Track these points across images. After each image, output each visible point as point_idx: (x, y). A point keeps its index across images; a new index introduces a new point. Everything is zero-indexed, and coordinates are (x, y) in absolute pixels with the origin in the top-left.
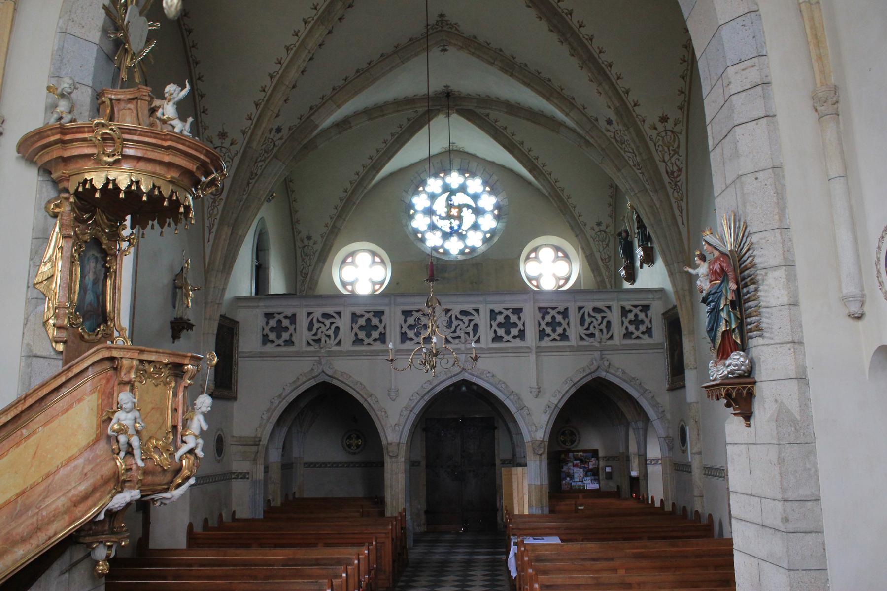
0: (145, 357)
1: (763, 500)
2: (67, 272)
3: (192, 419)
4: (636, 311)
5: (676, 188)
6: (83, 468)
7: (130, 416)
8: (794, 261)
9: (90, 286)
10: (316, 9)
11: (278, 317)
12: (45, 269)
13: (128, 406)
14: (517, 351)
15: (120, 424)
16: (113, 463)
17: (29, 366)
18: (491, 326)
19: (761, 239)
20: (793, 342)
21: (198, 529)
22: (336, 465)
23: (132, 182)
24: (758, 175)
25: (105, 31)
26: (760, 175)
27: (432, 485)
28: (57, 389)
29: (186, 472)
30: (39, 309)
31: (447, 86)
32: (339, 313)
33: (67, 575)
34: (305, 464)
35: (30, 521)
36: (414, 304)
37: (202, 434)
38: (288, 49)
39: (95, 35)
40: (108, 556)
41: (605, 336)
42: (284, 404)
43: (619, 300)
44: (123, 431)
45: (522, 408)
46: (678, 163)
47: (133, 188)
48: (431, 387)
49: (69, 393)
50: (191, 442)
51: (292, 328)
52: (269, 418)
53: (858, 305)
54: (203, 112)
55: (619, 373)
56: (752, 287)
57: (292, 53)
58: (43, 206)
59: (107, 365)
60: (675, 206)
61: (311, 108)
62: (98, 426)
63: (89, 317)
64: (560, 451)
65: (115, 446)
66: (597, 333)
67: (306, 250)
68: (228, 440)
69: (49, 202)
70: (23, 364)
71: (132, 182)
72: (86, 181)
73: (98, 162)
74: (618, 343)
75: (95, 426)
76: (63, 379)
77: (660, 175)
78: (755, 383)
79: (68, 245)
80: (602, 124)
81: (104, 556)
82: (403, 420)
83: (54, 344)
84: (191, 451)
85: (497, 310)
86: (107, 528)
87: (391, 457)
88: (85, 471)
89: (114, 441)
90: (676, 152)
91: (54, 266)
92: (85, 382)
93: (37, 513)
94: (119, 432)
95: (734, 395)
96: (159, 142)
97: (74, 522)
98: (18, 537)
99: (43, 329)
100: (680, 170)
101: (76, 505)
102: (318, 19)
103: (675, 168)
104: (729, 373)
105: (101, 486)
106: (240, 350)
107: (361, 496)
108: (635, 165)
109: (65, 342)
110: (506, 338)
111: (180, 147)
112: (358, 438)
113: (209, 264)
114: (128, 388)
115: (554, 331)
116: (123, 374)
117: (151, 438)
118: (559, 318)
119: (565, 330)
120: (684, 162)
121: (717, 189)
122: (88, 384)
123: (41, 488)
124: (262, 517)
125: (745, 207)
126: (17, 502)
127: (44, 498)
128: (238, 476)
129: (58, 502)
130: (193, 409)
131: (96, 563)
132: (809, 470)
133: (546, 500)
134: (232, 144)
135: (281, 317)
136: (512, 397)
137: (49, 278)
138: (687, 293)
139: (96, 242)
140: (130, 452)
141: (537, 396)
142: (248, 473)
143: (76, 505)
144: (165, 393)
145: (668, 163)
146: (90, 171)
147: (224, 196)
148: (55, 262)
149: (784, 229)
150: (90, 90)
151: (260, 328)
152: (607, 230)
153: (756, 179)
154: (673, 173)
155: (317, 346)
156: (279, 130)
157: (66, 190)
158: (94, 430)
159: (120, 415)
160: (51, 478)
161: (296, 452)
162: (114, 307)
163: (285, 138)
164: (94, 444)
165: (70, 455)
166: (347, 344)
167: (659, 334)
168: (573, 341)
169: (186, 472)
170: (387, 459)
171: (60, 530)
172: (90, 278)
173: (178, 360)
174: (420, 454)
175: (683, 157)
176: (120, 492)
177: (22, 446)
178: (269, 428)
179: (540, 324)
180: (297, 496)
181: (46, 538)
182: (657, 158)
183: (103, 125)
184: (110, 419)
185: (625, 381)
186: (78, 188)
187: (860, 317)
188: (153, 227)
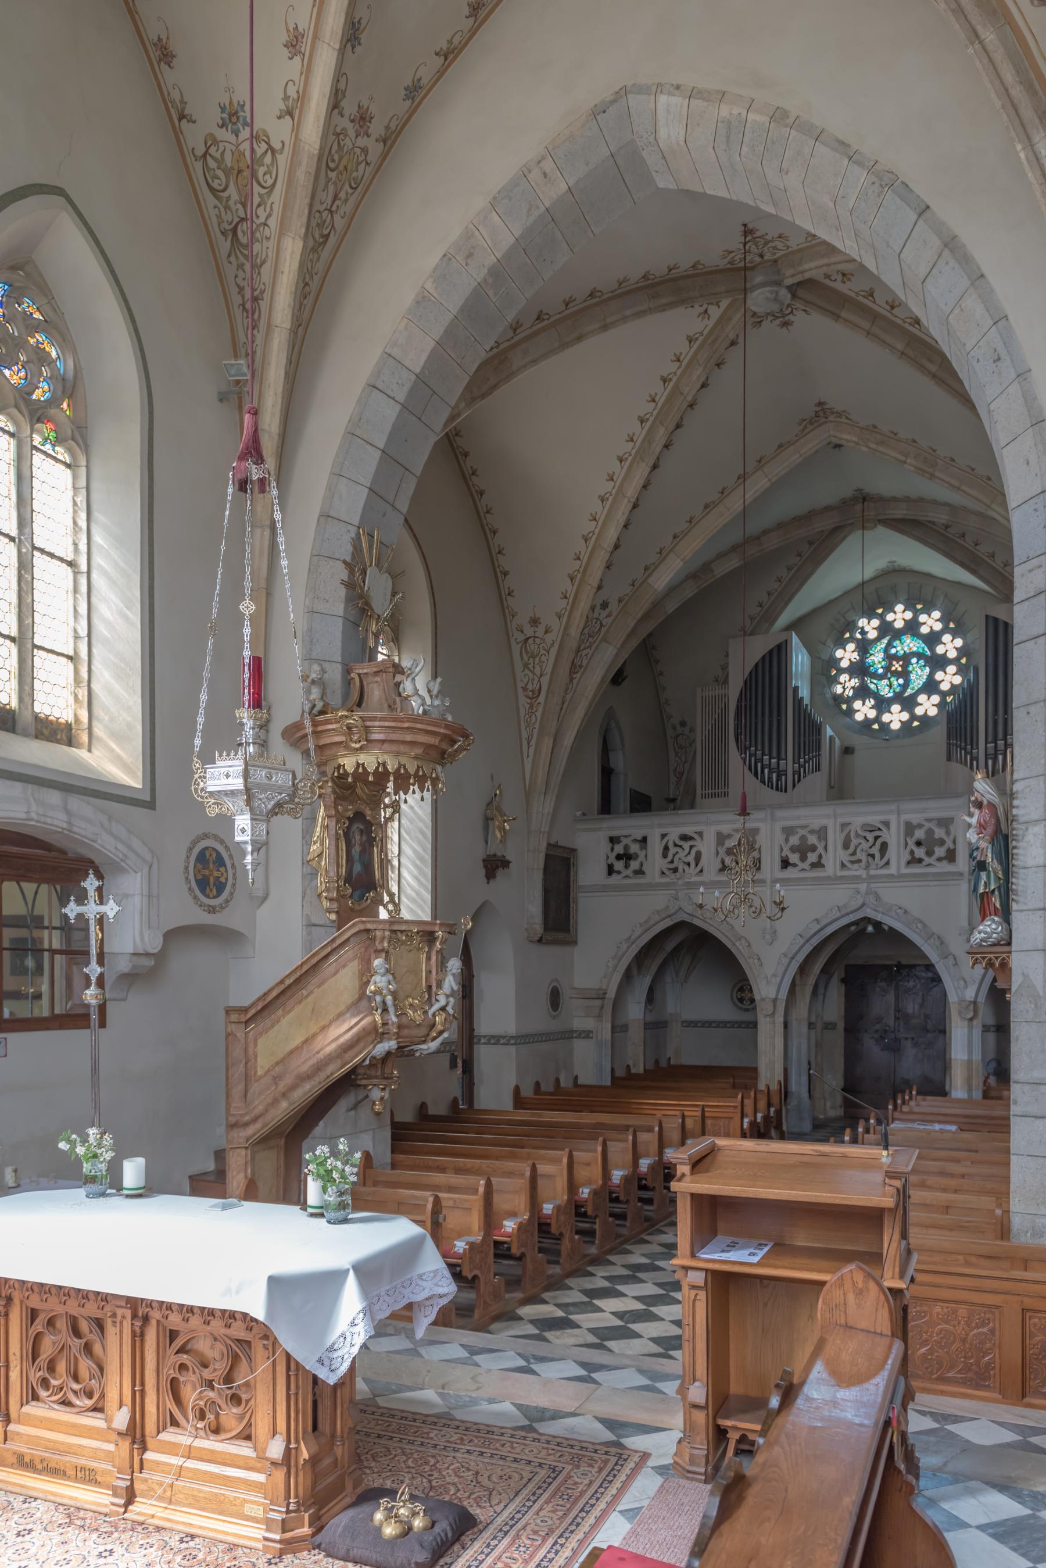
2: (333, 848)
7: (384, 979)
10: (632, 440)
13: (383, 970)
14: (940, 876)
17: (309, 933)
18: (906, 844)
21: (527, 1092)
25: (348, 600)
26: (1033, 709)
28: (326, 957)
29: (440, 1027)
30: (313, 884)
31: (859, 490)
32: (700, 834)
33: (353, 1113)
34: (683, 1022)
37: (453, 994)
38: (603, 499)
39: (339, 608)
40: (382, 1098)
42: (635, 950)
47: (380, 769)
48: (818, 927)
51: (642, 854)
54: (509, 594)
57: (608, 504)
59: (364, 936)
61: (646, 569)
67: (532, 646)
73: (347, 747)
76: (329, 949)
82: (782, 969)
84: (443, 1009)
85: (915, 822)
86: (379, 1073)
94: (375, 993)
96: (399, 725)
102: (637, 452)
106: (580, 883)
111: (419, 726)
117: (408, 997)
124: (609, 1083)
128: (580, 1035)
131: (374, 1103)
134: (546, 632)
139: (359, 816)
140: (385, 1010)
142: (592, 1032)
146: (342, 756)
147: (542, 699)
150: (339, 666)
155: (673, 876)
156: (605, 605)
159: (377, 978)
163: (615, 614)
165: (340, 1010)
177: (303, 1003)
178: (617, 978)
180: (672, 1063)
183: (346, 717)
184: (368, 982)
188: (414, 792)
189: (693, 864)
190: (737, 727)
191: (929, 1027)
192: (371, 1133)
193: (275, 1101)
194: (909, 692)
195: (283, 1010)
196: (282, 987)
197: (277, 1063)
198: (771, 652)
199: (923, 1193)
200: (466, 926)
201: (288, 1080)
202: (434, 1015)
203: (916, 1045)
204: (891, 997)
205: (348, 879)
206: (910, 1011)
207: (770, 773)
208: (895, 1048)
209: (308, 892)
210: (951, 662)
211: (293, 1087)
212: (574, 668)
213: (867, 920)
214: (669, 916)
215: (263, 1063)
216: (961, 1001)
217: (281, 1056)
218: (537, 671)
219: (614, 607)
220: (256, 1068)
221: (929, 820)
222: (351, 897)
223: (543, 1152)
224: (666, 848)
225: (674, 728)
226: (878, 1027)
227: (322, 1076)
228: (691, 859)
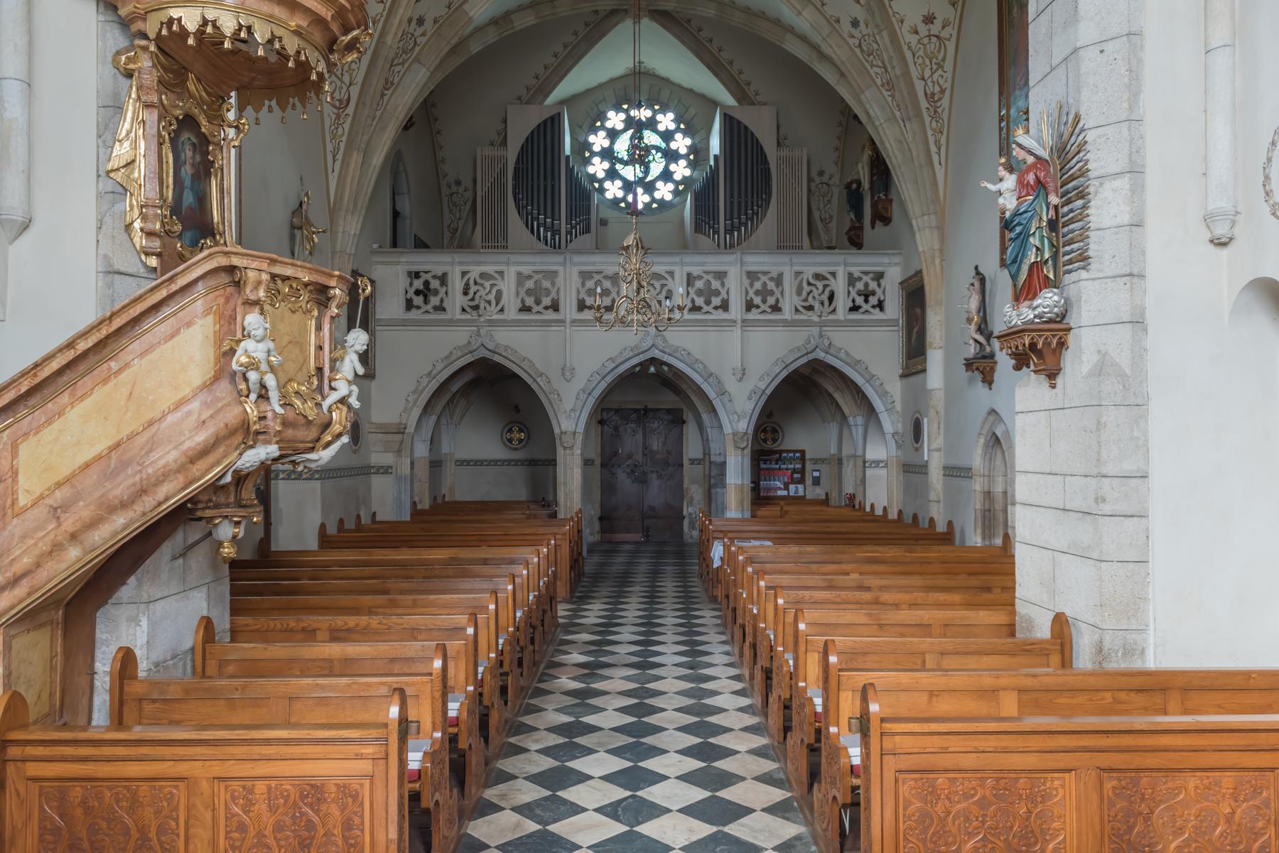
0: (277, 270)
1: (1068, 478)
3: (343, 359)
4: (866, 278)
5: (935, 115)
6: (200, 415)
7: (262, 347)
8: (1143, 166)
9: (188, 183)
11: (424, 277)
12: (122, 151)
14: (718, 323)
15: (249, 357)
16: (241, 409)
17: (110, 285)
19: (1099, 137)
20: (1131, 275)
21: (332, 530)
22: (495, 462)
23: (241, 26)
24: (1104, 46)
26: (1109, 47)
27: (608, 488)
29: (337, 428)
33: (181, 561)
35: (130, 481)
36: (594, 264)
40: (234, 537)
41: (827, 309)
42: (435, 385)
43: (846, 265)
44: (253, 365)
45: (722, 393)
46: (941, 81)
49: (174, 314)
50: (343, 389)
52: (416, 401)
53: (1227, 225)
55: (842, 355)
56: (1080, 203)
58: (110, 59)
60: (931, 140)
62: (217, 361)
63: (188, 223)
65: (243, 386)
66: (817, 305)
68: (365, 427)
69: (118, 53)
70: (100, 284)
71: (241, 26)
72: (171, 21)
74: (842, 318)
75: (212, 360)
76: (163, 293)
77: (916, 95)
78: (1070, 329)
79: (152, 117)
80: (846, 27)
81: (230, 535)
82: (580, 404)
83: (143, 257)
84: (343, 401)
86: (232, 499)
87: (565, 448)
88: (203, 417)
89: (239, 378)
90: (940, 66)
91: (135, 146)
92: (194, 301)
93: (140, 471)
95: (1040, 346)
97: (191, 483)
98: (116, 502)
99: (125, 236)
100: (943, 91)
101: (192, 461)
103: (937, 89)
104: (1035, 317)
105: (226, 438)
107: (523, 498)
108: (883, 85)
109: (159, 255)
110: (706, 308)
112: (521, 431)
113: (335, 204)
114: (257, 309)
115: (764, 301)
116: (248, 291)
117: (290, 380)
118: (771, 285)
119: (777, 301)
120: (950, 80)
121: (1034, 77)
122: (199, 302)
123: (140, 440)
124: (408, 519)
125: (1079, 92)
126: (110, 458)
127: (151, 450)
129: (168, 456)
130: (344, 347)
131: (220, 544)
133: (747, 503)
135: (428, 277)
136: (711, 380)
137: (128, 165)
138: (937, 254)
139: (188, 122)
140: (263, 396)
141: (741, 380)
143: (192, 461)
144: (306, 325)
145: (929, 82)
148: (136, 144)
149: (1133, 121)
151: (402, 291)
152: (831, 182)
153: (1102, 51)
154: (933, 94)
155: (475, 313)
157: (144, 36)
158: (212, 365)
159: (248, 344)
160: (155, 428)
161: (445, 448)
162: (223, 218)
163: (429, 35)
164: (212, 383)
165: (180, 396)
166: (512, 313)
167: (894, 309)
168: (787, 314)
169: (337, 428)
170: (560, 452)
171: (171, 494)
172: (187, 171)
173: (322, 280)
174: (594, 453)
175: (949, 75)
176: (252, 447)
177: (110, 385)
178: (416, 412)
179: (747, 293)
181: (155, 503)
182: (914, 73)
184: (232, 352)
185: (848, 364)
186: (160, 30)
187: (1221, 243)
189: (494, 303)
190: (515, 187)
191: (670, 461)
192: (204, 589)
193: (57, 548)
194: (649, 179)
195: (72, 395)
196: (71, 355)
197: (59, 485)
198: (545, 122)
199: (918, 612)
200: (364, 290)
201: (84, 511)
202: (330, 411)
203: (660, 477)
204: (639, 436)
205: (176, 209)
206: (655, 448)
207: (546, 231)
208: (643, 480)
209: (107, 219)
210: (682, 157)
211: (94, 524)
212: (388, 84)
213: (653, 360)
214: (471, 352)
215: (29, 486)
216: (735, 434)
217: (65, 472)
218: (346, 79)
219: (428, 24)
220: (14, 492)
221: (708, 273)
222: (180, 237)
223: (433, 597)
224: (467, 285)
225: (450, 187)
226: (629, 462)
227: (148, 502)
228: (492, 297)
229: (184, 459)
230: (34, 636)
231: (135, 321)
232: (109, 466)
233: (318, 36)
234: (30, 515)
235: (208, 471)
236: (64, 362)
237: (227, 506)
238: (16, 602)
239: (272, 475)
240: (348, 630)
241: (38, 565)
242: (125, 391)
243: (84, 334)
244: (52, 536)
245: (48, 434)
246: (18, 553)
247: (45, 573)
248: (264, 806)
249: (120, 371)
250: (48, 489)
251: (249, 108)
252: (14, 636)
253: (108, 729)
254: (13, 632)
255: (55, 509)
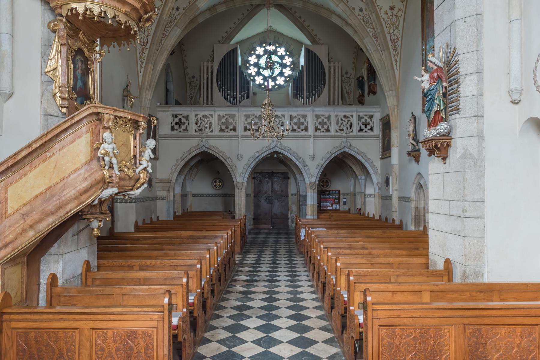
0: (117, 114)
1: (451, 202)
3: (145, 152)
4: (366, 118)
5: (395, 48)
6: (84, 175)
7: (111, 146)
8: (483, 70)
9: (79, 77)
11: (179, 117)
12: (51, 64)
14: (303, 136)
15: (105, 151)
16: (102, 173)
17: (47, 120)
19: (464, 58)
20: (477, 116)
21: (140, 224)
22: (209, 195)
23: (102, 11)
24: (466, 20)
26: (468, 20)
27: (257, 206)
29: (142, 181)
33: (76, 237)
35: (55, 203)
36: (251, 111)
40: (99, 227)
41: (349, 130)
42: (183, 162)
43: (357, 112)
44: (107, 154)
45: (305, 166)
46: (397, 34)
49: (74, 132)
50: (145, 164)
52: (176, 169)
53: (518, 95)
55: (356, 150)
56: (456, 86)
58: (46, 25)
60: (393, 59)
62: (92, 152)
63: (80, 94)
64: (323, 190)
65: (102, 163)
66: (345, 129)
68: (154, 180)
69: (50, 22)
70: (42, 120)
71: (102, 11)
72: (72, 9)
74: (355, 134)
75: (90, 152)
76: (69, 124)
77: (387, 40)
78: (452, 139)
79: (64, 49)
80: (357, 11)
81: (97, 226)
82: (245, 170)
83: (60, 108)
84: (145, 169)
86: (98, 211)
87: (239, 189)
88: (86, 176)
89: (101, 160)
90: (397, 28)
91: (57, 62)
92: (82, 127)
93: (59, 199)
95: (439, 146)
97: (81, 204)
98: (49, 212)
99: (53, 100)
100: (398, 39)
101: (81, 194)
103: (396, 37)
104: (437, 134)
105: (95, 185)
107: (221, 210)
108: (373, 36)
109: (67, 108)
110: (298, 130)
112: (220, 182)
113: (141, 86)
114: (108, 131)
115: (323, 127)
116: (105, 123)
117: (123, 160)
118: (326, 120)
119: (328, 127)
120: (401, 34)
121: (436, 33)
122: (84, 128)
123: (59, 186)
124: (172, 219)
125: (456, 39)
126: (46, 193)
127: (64, 190)
129: (71, 192)
130: (145, 147)
131: (93, 230)
132: (480, 185)
133: (316, 212)
135: (181, 117)
136: (300, 160)
137: (54, 69)
138: (396, 107)
139: (80, 51)
140: (111, 167)
141: (313, 160)
143: (81, 194)
144: (129, 137)
145: (392, 35)
148: (58, 61)
149: (478, 51)
151: (170, 123)
152: (351, 77)
153: (465, 22)
154: (394, 40)
155: (200, 132)
157: (61, 15)
158: (89, 154)
159: (105, 145)
160: (65, 181)
161: (188, 189)
162: (94, 92)
163: (181, 15)
164: (89, 162)
165: (76, 167)
166: (216, 132)
167: (378, 130)
168: (332, 132)
169: (142, 181)
170: (236, 191)
171: (72, 208)
172: (79, 72)
173: (136, 118)
174: (251, 191)
175: (401, 32)
176: (106, 189)
177: (47, 162)
178: (176, 174)
179: (315, 123)
181: (65, 212)
182: (386, 31)
184: (98, 148)
185: (358, 154)
186: (68, 13)
187: (515, 103)
189: (208, 128)
190: (217, 79)
191: (283, 195)
192: (86, 249)
193: (24, 231)
194: (274, 75)
195: (30, 167)
196: (30, 150)
197: (25, 205)
198: (230, 51)
199: (388, 258)
200: (154, 123)
201: (35, 216)
202: (139, 173)
203: (279, 201)
204: (270, 184)
205: (74, 88)
206: (277, 189)
207: (230, 98)
208: (271, 203)
209: (45, 93)
210: (288, 66)
211: (39, 221)
212: (164, 35)
213: (276, 152)
214: (199, 149)
215: (12, 205)
216: (310, 183)
217: (27, 199)
218: (146, 33)
219: (181, 10)
220: (6, 208)
221: (299, 115)
222: (76, 100)
223: (183, 252)
224: (197, 120)
225: (190, 79)
226: (266, 195)
227: (63, 212)
228: (208, 125)
229: (78, 194)
230: (14, 268)
231: (57, 136)
232: (46, 197)
233: (134, 15)
234: (13, 217)
235: (88, 199)
236: (27, 153)
237: (96, 213)
238: (7, 254)
239: (115, 201)
240: (147, 266)
241: (16, 239)
242: (53, 165)
243: (35, 141)
244: (22, 226)
245: (20, 183)
246: (7, 233)
247: (19, 242)
248: (112, 340)
249: (51, 156)
250: (20, 206)
251: (105, 45)
252: (6, 269)
253: (46, 308)
254: (5, 267)
255: (23, 215)
